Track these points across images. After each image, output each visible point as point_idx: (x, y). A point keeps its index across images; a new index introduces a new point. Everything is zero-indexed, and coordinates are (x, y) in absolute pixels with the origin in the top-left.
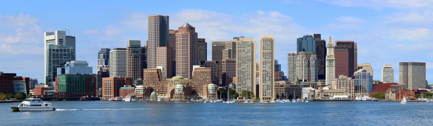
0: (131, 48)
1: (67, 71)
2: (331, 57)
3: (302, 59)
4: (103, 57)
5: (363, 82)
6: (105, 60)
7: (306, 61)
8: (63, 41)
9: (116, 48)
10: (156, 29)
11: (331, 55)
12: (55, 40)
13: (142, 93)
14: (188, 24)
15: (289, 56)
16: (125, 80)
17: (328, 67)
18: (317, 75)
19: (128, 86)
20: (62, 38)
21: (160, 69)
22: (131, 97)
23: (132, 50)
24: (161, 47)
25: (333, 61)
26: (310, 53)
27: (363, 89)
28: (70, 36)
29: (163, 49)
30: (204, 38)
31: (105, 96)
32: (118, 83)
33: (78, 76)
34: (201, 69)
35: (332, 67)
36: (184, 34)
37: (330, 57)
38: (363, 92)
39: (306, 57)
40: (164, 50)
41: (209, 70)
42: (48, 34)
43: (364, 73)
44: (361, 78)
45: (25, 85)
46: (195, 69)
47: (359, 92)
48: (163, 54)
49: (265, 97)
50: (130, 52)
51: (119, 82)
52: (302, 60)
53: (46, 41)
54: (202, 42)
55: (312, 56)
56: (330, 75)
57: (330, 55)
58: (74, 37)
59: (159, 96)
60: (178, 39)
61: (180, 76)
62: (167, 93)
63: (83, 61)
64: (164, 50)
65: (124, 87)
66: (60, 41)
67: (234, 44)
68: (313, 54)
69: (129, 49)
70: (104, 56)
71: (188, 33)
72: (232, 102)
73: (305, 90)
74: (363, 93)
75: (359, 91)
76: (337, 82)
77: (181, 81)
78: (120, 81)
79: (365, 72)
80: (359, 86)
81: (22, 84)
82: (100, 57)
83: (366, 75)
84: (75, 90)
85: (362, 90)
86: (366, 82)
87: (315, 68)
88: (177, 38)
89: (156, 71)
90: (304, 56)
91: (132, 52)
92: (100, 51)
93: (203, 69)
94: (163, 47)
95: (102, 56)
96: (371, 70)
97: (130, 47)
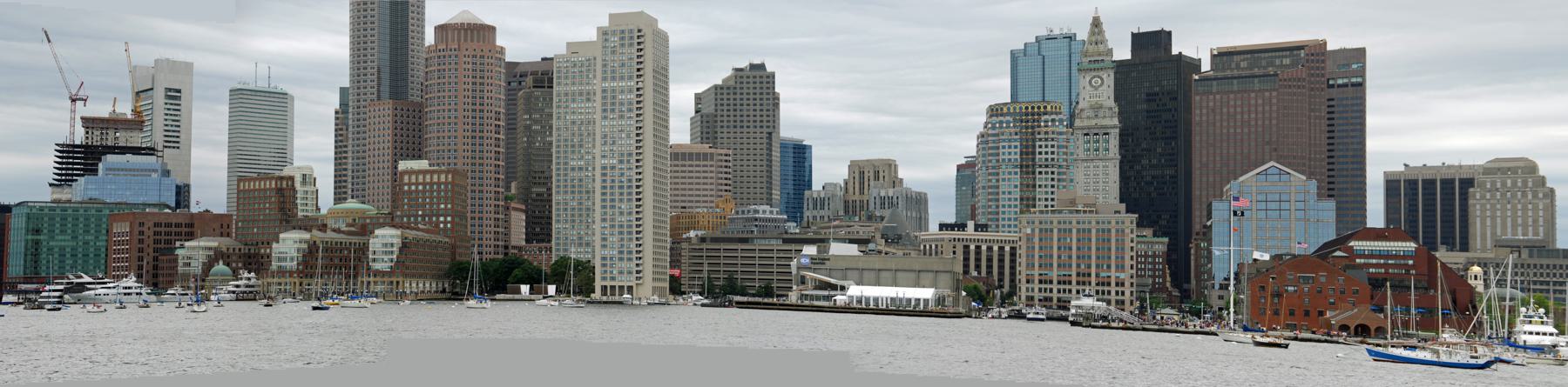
11: (1097, 108)
26: (1036, 110)
32: (156, 233)
49: (613, 283)
51: (163, 229)
55: (1046, 121)
60: (431, 122)
66: (169, 94)
71: (457, 47)
78: (169, 225)
88: (430, 119)
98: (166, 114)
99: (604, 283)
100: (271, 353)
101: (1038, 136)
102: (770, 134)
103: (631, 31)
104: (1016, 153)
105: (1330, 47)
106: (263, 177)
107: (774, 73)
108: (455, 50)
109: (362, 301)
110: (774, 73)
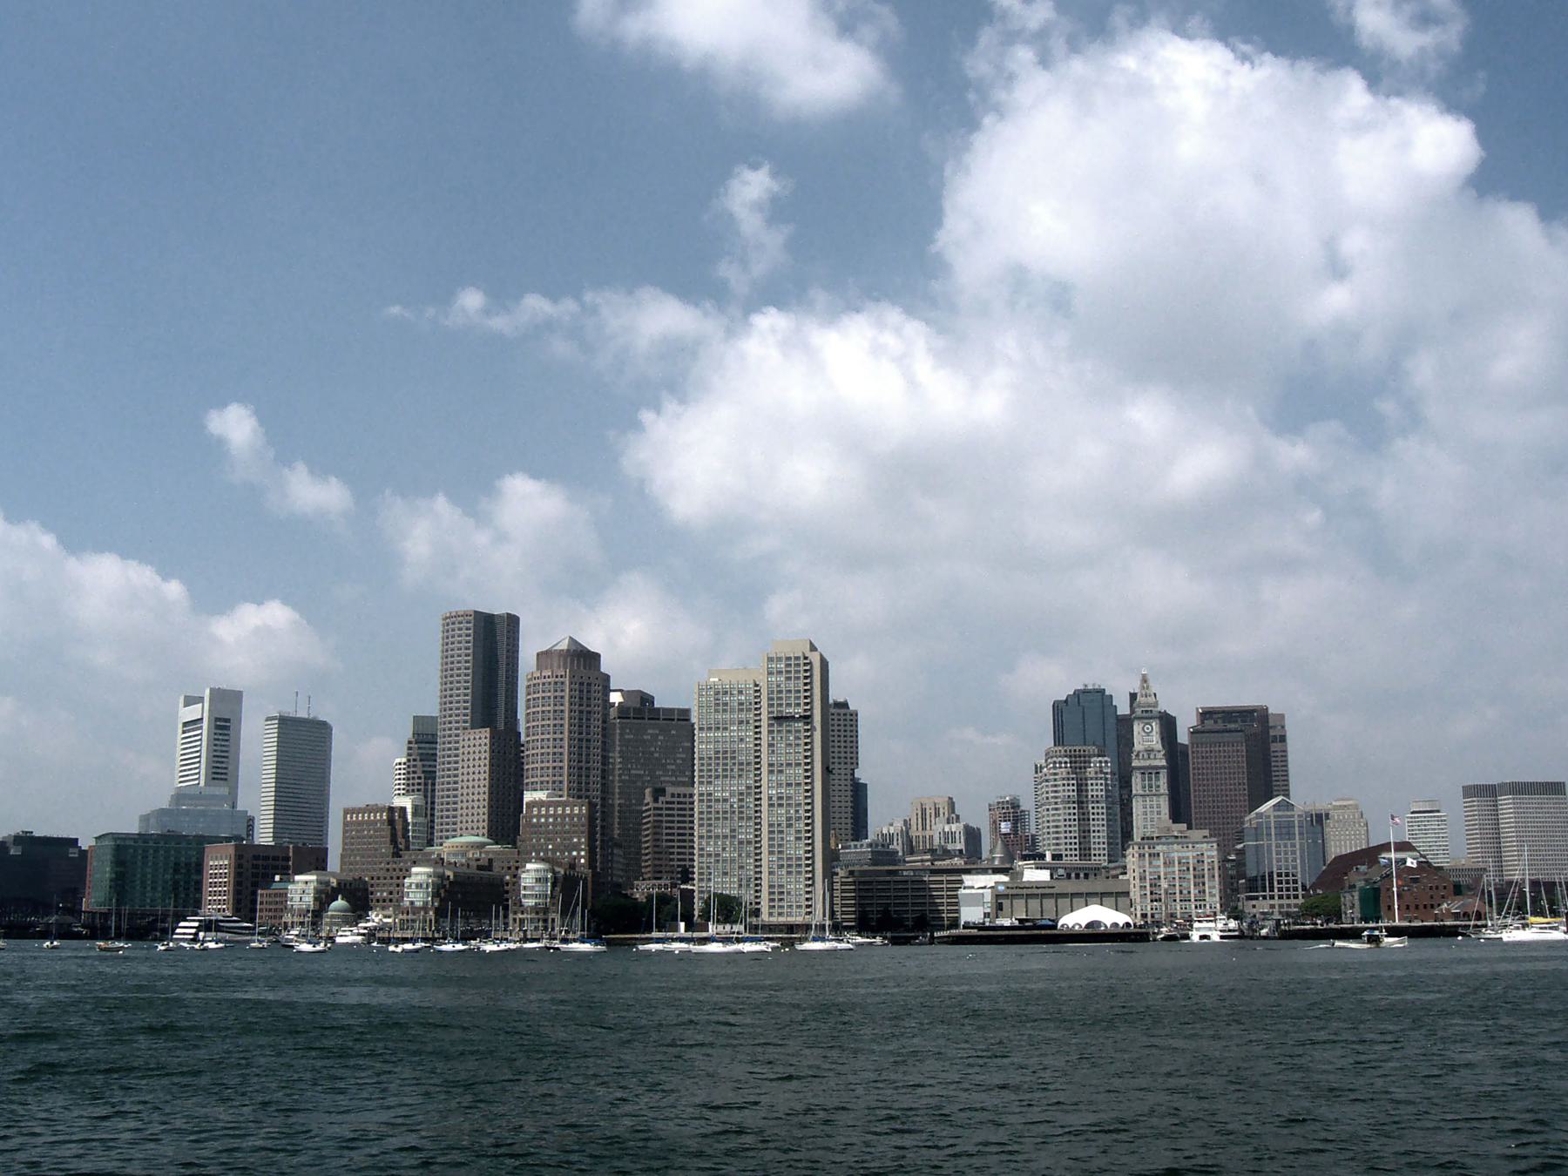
2: (1152, 756)
5: (1278, 853)
7: (1099, 782)
8: (288, 726)
11: (1149, 751)
13: (309, 900)
14: (576, 642)
15: (1036, 772)
16: (291, 854)
18: (1117, 838)
21: (403, 810)
23: (420, 751)
25: (1158, 773)
27: (1280, 882)
30: (686, 707)
33: (166, 843)
35: (1155, 798)
37: (1146, 756)
38: (1281, 897)
41: (580, 810)
43: (1280, 813)
44: (1269, 835)
47: (1264, 898)
51: (260, 862)
54: (678, 720)
57: (1147, 751)
58: (538, 654)
61: (478, 835)
68: (1099, 756)
72: (399, 950)
73: (973, 887)
74: (1281, 902)
75: (1265, 891)
76: (1142, 851)
78: (266, 858)
79: (1288, 810)
80: (1264, 876)
83: (1290, 825)
84: (183, 896)
85: (1276, 890)
86: (1294, 853)
87: (1104, 811)
90: (1060, 763)
91: (418, 758)
93: (564, 805)
96: (1359, 823)
98: (215, 745)
100: (589, 1038)
101: (1075, 782)
102: (853, 770)
103: (797, 658)
106: (370, 809)
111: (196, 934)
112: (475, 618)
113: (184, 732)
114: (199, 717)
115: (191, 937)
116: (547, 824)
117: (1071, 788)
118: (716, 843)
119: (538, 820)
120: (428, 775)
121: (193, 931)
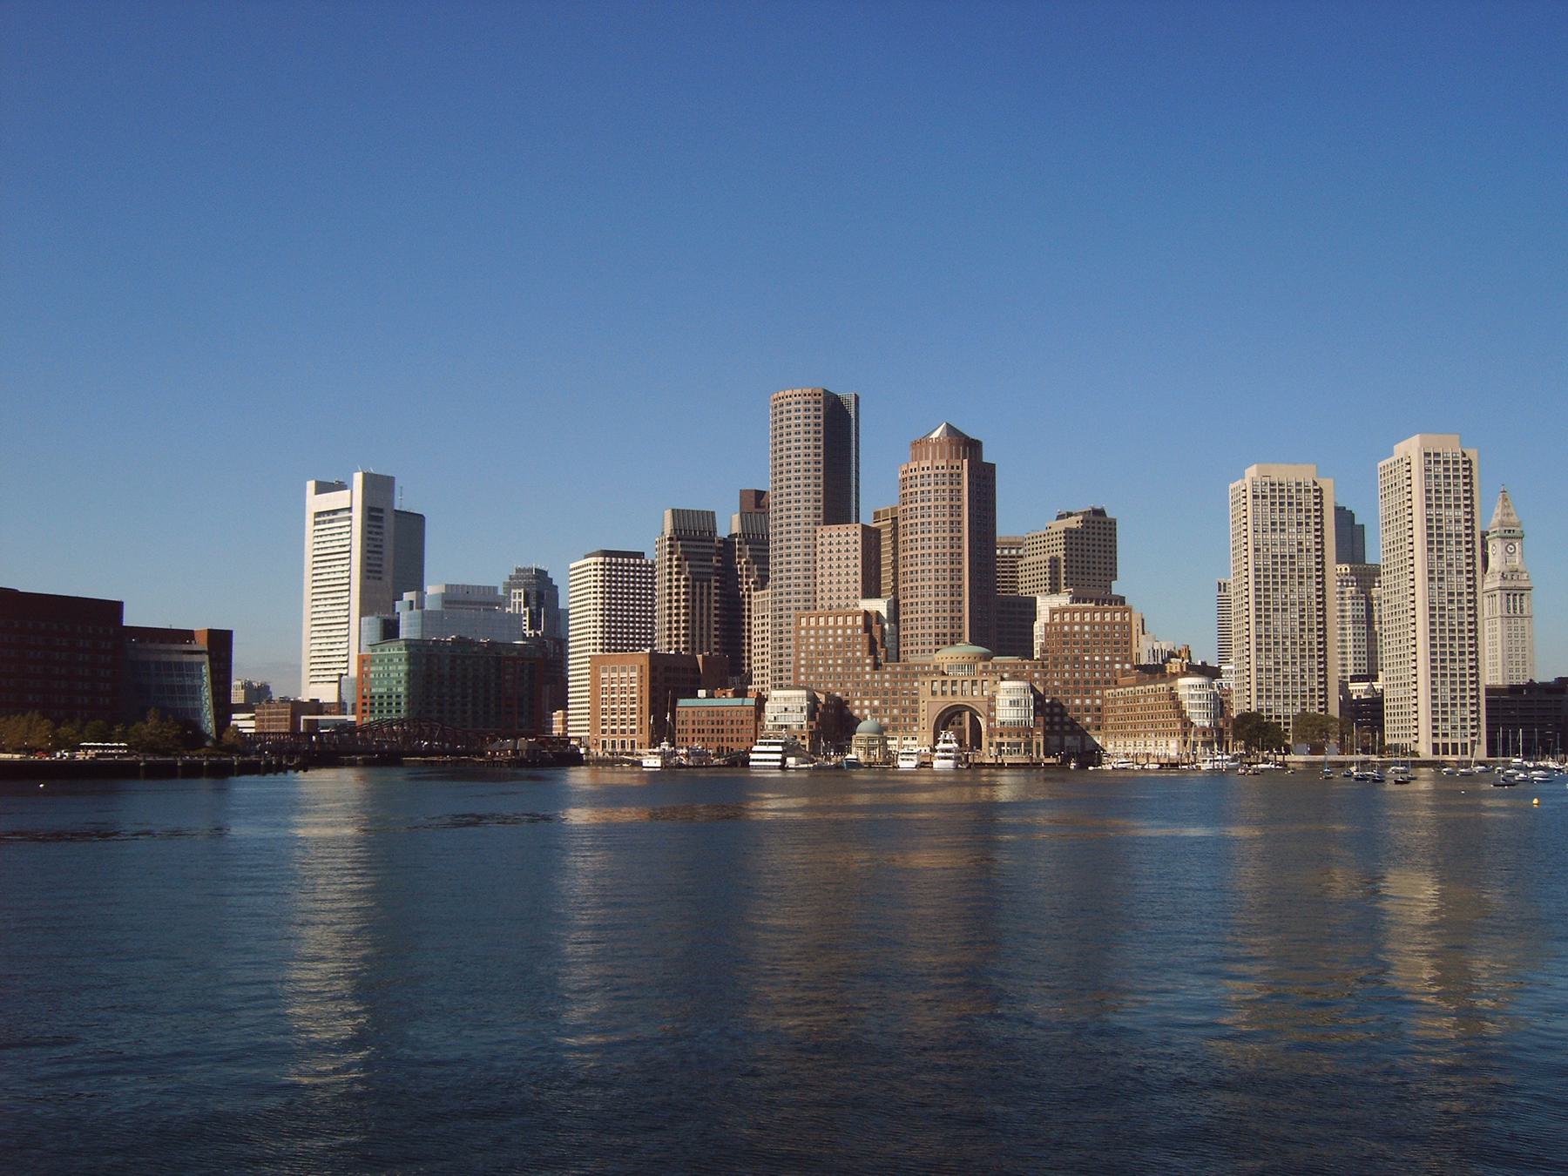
0: (678, 539)
1: (408, 628)
3: (1342, 593)
4: (522, 600)
6: (530, 611)
8: (382, 517)
9: (599, 549)
10: (802, 455)
12: (350, 509)
15: (1220, 590)
17: (1505, 621)
19: (718, 692)
20: (379, 506)
22: (779, 748)
24: (829, 526)
28: (403, 510)
29: (843, 533)
31: (604, 742)
34: (1075, 611)
36: (943, 468)
37: (1509, 577)
39: (1355, 584)
40: (851, 539)
42: (322, 488)
45: (205, 670)
46: (1054, 614)
48: (843, 557)
50: (675, 556)
52: (1342, 599)
53: (315, 517)
56: (1514, 660)
59: (895, 742)
62: (918, 725)
63: (479, 587)
64: (851, 539)
65: (696, 696)
66: (373, 514)
67: (1110, 529)
69: (671, 546)
70: (527, 596)
71: (959, 464)
77: (985, 667)
81: (190, 666)
82: (513, 600)
89: (860, 620)
91: (683, 557)
92: (510, 576)
94: (842, 526)
95: (520, 597)
97: (674, 536)
99: (1436, 741)
104: (1362, 610)
105: (130, 619)
107: (1115, 520)
108: (958, 468)
109: (585, 882)
110: (1115, 520)
111: (783, 761)
112: (825, 399)
113: (316, 523)
114: (349, 506)
115: (779, 764)
116: (1082, 633)
117: (1360, 607)
118: (1267, 657)
119: (1071, 628)
120: (695, 577)
121: (779, 756)
